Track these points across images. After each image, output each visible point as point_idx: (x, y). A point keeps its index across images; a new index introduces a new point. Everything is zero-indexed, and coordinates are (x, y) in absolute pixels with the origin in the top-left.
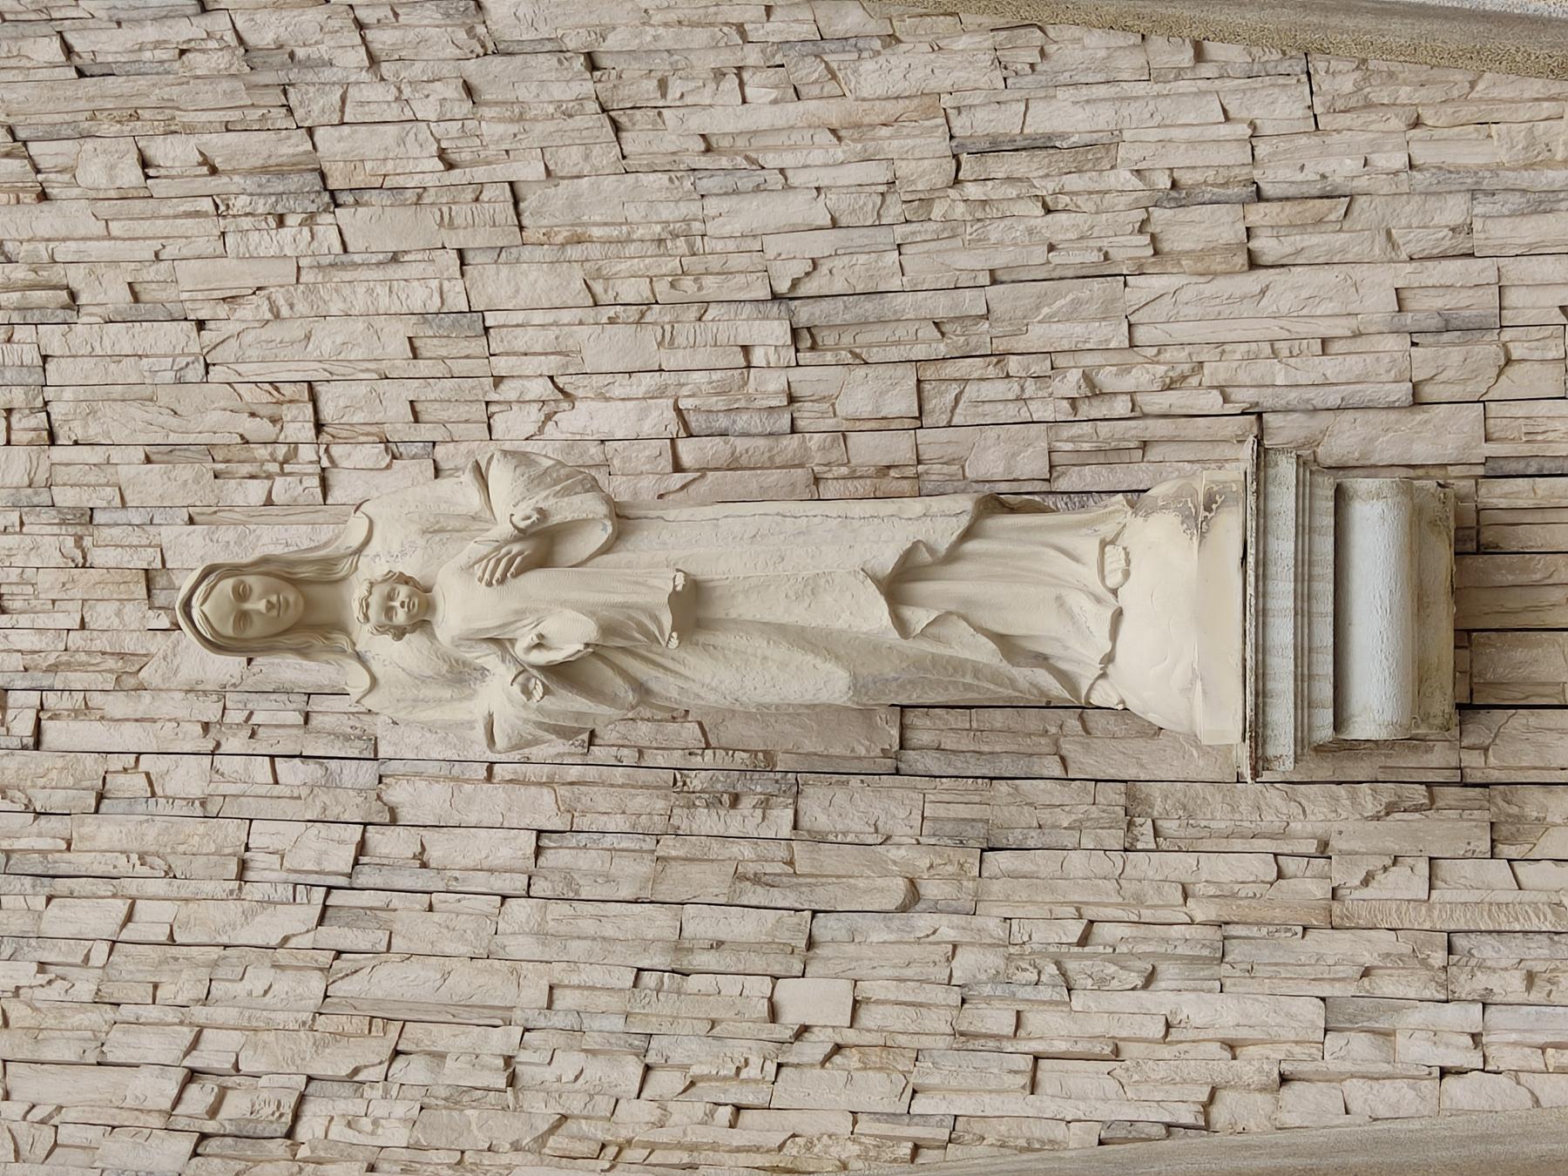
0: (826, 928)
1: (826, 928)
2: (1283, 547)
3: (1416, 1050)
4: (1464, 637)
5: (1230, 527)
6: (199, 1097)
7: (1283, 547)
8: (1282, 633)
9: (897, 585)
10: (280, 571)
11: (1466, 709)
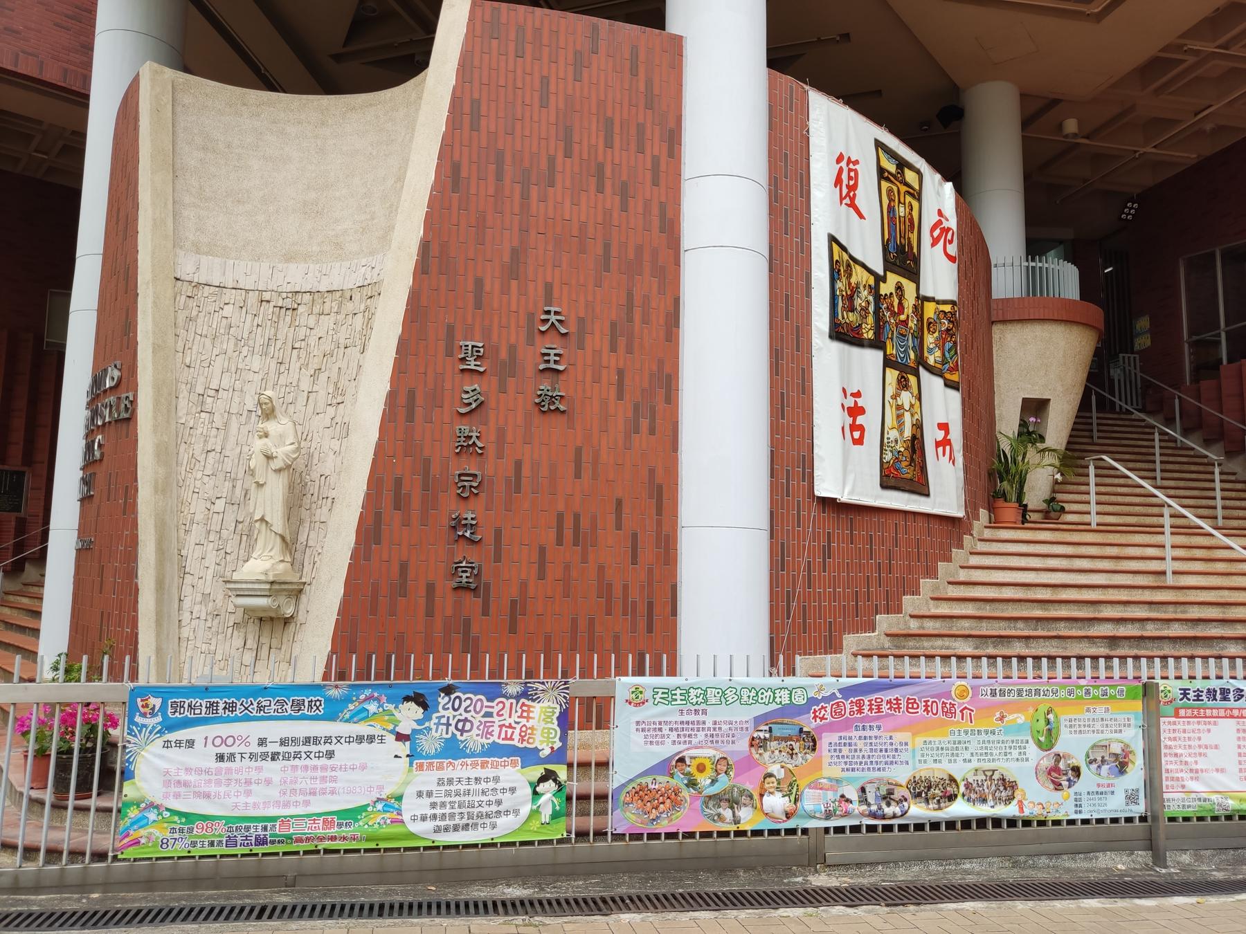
0: (236, 507)
1: (236, 507)
2: (256, 586)
3: (197, 608)
4: (272, 619)
5: (263, 578)
6: (212, 393)
7: (256, 586)
8: (244, 586)
9: (262, 520)
10: (273, 410)
11: (261, 619)
